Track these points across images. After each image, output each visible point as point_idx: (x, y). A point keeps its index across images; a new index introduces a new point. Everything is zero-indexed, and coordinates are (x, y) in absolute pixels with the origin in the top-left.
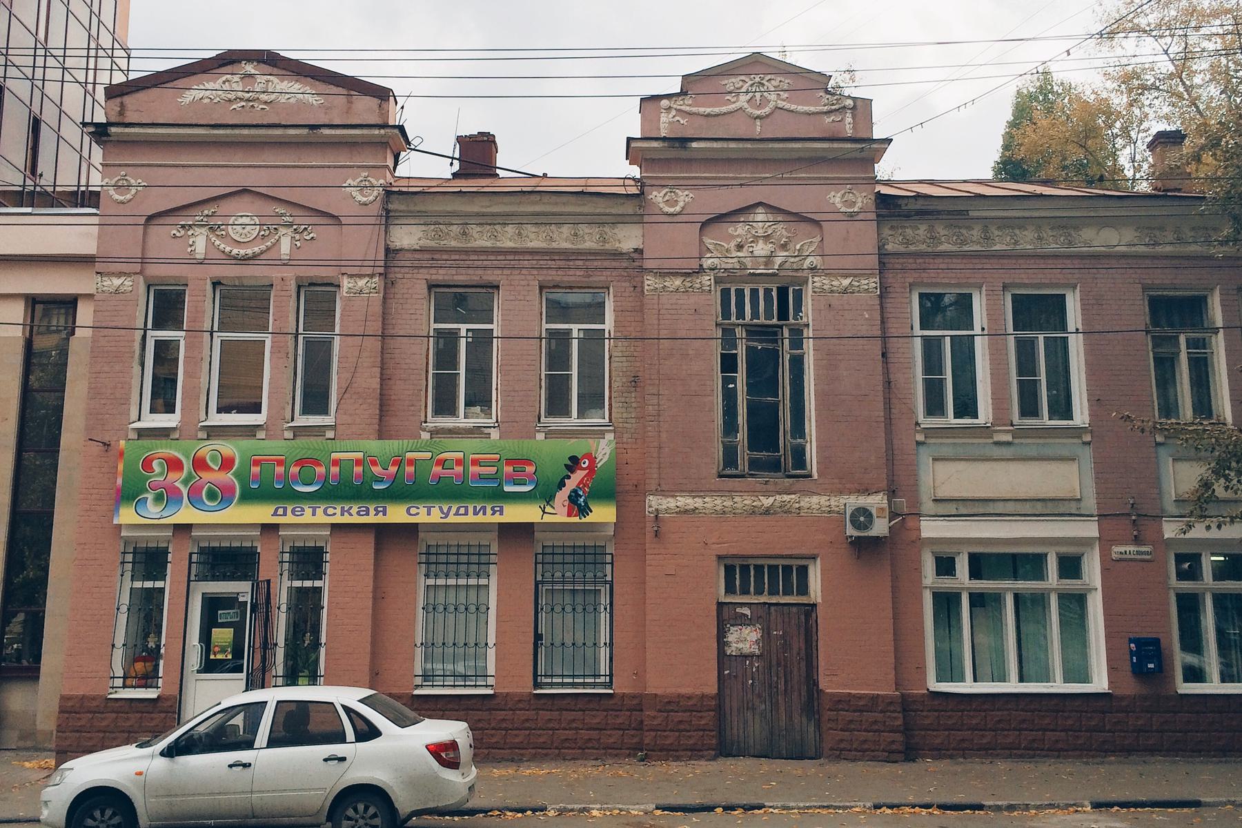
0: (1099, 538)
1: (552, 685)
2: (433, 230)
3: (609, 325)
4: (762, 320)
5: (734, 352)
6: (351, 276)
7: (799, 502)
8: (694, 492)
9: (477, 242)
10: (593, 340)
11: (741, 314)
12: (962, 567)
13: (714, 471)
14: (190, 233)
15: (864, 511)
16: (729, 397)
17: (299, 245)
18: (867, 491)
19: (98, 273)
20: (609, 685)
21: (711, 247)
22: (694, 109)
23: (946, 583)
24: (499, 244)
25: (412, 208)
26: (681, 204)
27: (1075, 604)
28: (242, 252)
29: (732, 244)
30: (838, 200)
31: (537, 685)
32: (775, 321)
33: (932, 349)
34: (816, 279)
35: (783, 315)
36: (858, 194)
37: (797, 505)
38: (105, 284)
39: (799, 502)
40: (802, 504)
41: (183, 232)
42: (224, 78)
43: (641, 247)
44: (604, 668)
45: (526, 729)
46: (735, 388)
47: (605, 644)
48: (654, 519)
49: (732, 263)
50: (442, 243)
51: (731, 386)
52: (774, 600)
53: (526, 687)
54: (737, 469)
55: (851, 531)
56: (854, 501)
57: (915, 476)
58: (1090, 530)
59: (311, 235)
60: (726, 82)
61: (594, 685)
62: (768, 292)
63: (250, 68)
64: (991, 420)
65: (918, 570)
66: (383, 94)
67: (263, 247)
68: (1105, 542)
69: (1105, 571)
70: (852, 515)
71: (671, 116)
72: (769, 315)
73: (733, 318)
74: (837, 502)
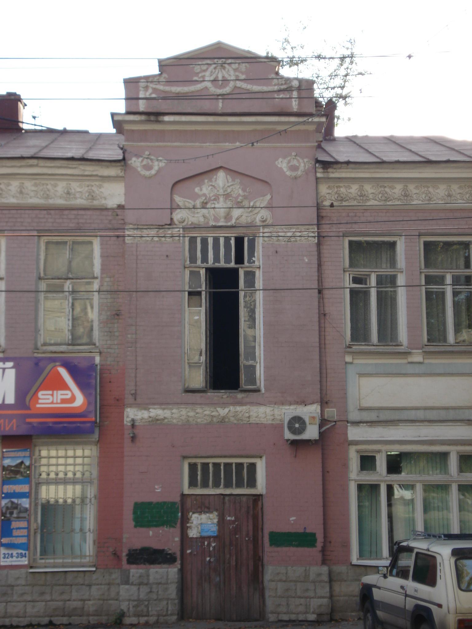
4: (222, 264)
8: (163, 404)
11: (205, 259)
23: (368, 478)
26: (156, 168)
29: (198, 203)
32: (232, 265)
35: (240, 259)
40: (251, 414)
52: (228, 491)
55: (288, 435)
65: (345, 466)
72: (228, 260)
73: (199, 262)
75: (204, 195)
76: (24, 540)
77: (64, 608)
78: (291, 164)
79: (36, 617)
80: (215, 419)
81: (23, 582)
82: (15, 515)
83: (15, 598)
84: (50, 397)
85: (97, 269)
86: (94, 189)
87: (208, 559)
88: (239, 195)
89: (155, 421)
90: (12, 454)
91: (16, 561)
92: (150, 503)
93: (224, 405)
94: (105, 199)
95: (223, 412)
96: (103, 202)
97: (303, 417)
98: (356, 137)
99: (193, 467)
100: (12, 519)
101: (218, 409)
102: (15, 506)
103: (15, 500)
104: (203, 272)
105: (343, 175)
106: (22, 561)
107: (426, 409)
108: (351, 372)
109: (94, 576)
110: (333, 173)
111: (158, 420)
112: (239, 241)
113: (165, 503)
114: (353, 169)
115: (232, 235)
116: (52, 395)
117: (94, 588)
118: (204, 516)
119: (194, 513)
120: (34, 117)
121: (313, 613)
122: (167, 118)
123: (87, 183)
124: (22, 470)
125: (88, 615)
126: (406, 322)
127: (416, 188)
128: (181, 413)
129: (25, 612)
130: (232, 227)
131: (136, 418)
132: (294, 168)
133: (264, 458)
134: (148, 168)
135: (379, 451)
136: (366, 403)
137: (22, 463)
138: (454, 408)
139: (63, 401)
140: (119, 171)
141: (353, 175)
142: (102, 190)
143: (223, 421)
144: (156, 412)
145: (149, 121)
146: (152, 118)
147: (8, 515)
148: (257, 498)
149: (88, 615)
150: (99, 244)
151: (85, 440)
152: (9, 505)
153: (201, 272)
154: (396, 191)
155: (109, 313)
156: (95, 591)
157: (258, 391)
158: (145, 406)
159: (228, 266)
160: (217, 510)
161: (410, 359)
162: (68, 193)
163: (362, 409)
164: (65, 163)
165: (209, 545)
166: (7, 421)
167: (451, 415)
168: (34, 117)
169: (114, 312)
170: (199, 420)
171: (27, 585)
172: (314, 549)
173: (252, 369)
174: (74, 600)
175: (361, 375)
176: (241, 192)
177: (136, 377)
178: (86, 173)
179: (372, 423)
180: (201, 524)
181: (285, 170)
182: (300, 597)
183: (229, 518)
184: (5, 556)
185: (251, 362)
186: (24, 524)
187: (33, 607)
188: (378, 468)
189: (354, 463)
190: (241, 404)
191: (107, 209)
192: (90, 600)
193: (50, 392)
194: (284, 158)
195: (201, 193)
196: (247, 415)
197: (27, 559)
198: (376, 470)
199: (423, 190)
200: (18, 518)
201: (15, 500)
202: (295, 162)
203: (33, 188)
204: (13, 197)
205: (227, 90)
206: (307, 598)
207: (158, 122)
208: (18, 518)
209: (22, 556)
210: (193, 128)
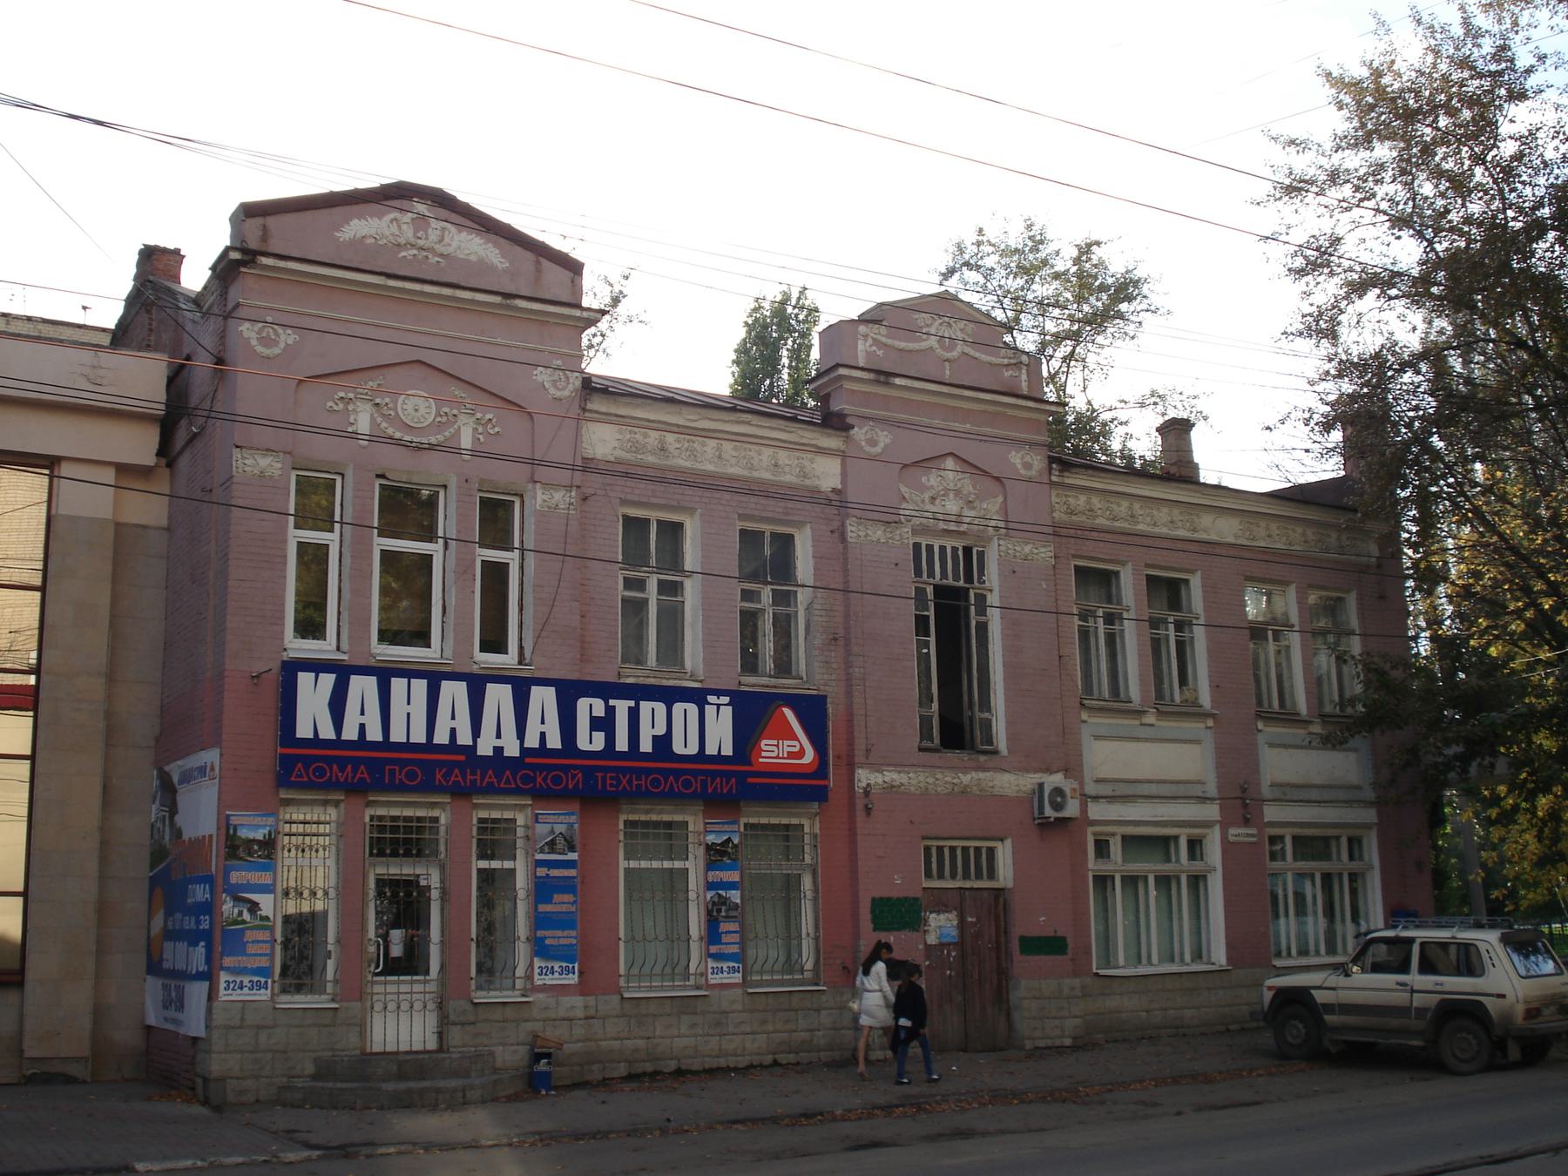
0: (168, 529)
2: (629, 441)
4: (950, 581)
5: (926, 613)
6: (545, 485)
7: (992, 781)
8: (899, 766)
9: (675, 461)
11: (931, 574)
12: (1116, 848)
14: (351, 407)
16: (924, 660)
17: (482, 440)
19: (237, 447)
22: (890, 342)
23: (1104, 867)
24: (698, 466)
26: (882, 445)
27: (1197, 881)
29: (927, 496)
32: (961, 583)
34: (1001, 542)
35: (969, 579)
37: (991, 784)
38: (247, 462)
39: (992, 781)
40: (995, 782)
41: (341, 406)
42: (392, 216)
43: (839, 487)
47: (808, 935)
48: (863, 795)
50: (639, 457)
52: (968, 884)
54: (933, 742)
58: (1212, 812)
60: (917, 316)
62: (955, 550)
63: (421, 208)
68: (1225, 825)
69: (1224, 852)
72: (957, 578)
74: (1028, 781)
75: (932, 487)
76: (735, 949)
77: (671, 1048)
79: (758, 1054)
80: (956, 789)
81: (740, 1007)
82: (723, 914)
83: (731, 1029)
84: (775, 748)
86: (806, 463)
87: (948, 972)
88: (970, 493)
89: (890, 788)
90: (717, 828)
91: (249, 994)
92: (889, 899)
93: (965, 770)
94: (819, 479)
95: (966, 779)
96: (817, 482)
97: (1064, 788)
98: (168, 377)
100: (721, 919)
101: (960, 775)
102: (723, 901)
103: (722, 893)
104: (930, 590)
105: (1078, 482)
106: (260, 995)
107: (1159, 782)
108: (1086, 732)
109: (824, 998)
110: (1068, 477)
111: (893, 786)
112: (968, 551)
113: (906, 898)
114: (1088, 476)
115: (959, 544)
116: (777, 746)
117: (824, 1013)
118: (942, 917)
119: (931, 913)
121: (1069, 1037)
122: (898, 381)
123: (797, 454)
124: (730, 850)
125: (819, 1050)
126: (1137, 673)
127: (1141, 508)
128: (920, 778)
129: (744, 1048)
131: (872, 782)
132: (1028, 466)
135: (1113, 835)
137: (729, 840)
139: (791, 755)
140: (841, 444)
141: (1088, 484)
142: (814, 465)
143: (965, 791)
144: (891, 776)
145: (878, 382)
146: (882, 378)
147: (715, 914)
148: (999, 892)
149: (819, 1050)
150: (809, 544)
151: (803, 811)
152: (716, 899)
153: (928, 590)
154: (1122, 509)
155: (824, 637)
156: (825, 1018)
157: (995, 752)
158: (877, 767)
159: (956, 584)
160: (955, 909)
162: (776, 465)
163: (1098, 781)
164: (782, 423)
165: (949, 953)
166: (479, 784)
167: (1181, 790)
169: (831, 637)
170: (939, 789)
171: (744, 1011)
172: (1065, 957)
173: (987, 725)
174: (801, 1031)
175: (1097, 738)
176: (971, 489)
177: (866, 727)
179: (1111, 799)
180: (940, 927)
182: (1055, 1018)
183: (970, 919)
184: (228, 985)
185: (986, 715)
186: (734, 926)
187: (754, 1040)
188: (1112, 856)
190: (985, 769)
192: (629, 1039)
193: (775, 742)
195: (928, 484)
197: (740, 975)
198: (1109, 857)
199: (1147, 511)
200: (726, 917)
201: (722, 893)
202: (1028, 459)
205: (954, 354)
206: (1061, 1018)
207: (887, 384)
208: (726, 917)
209: (734, 970)
210: (927, 398)
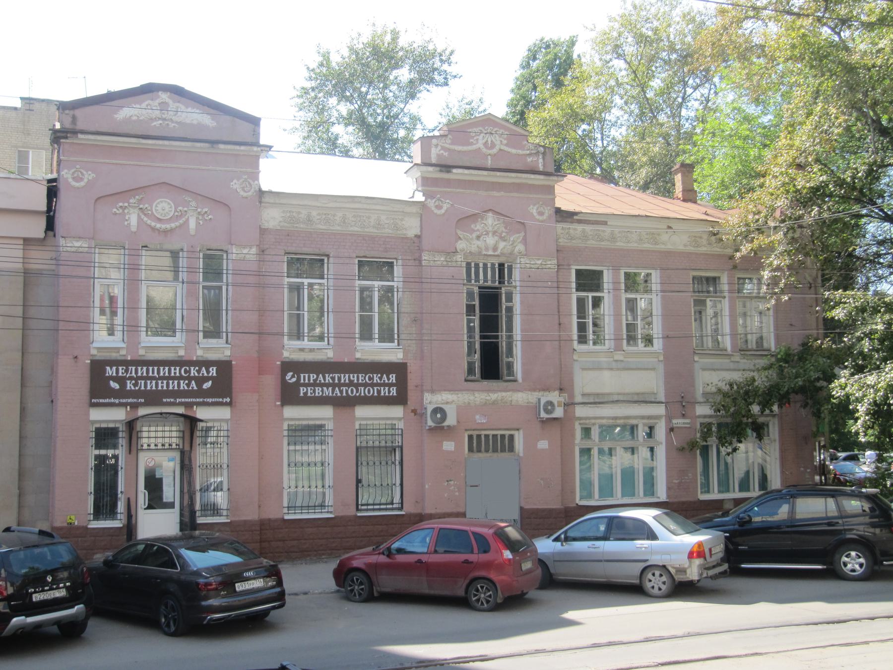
1: (367, 510)
3: (397, 282)
4: (489, 283)
10: (387, 295)
13: (463, 379)
15: (551, 403)
18: (546, 389)
20: (401, 509)
21: (461, 236)
23: (587, 444)
25: (277, 201)
28: (163, 226)
29: (474, 235)
30: (535, 211)
31: (358, 509)
33: (581, 303)
36: (85, 173)
41: (121, 211)
44: (397, 499)
45: (353, 537)
46: (474, 326)
49: (474, 249)
51: (472, 324)
53: (351, 511)
55: (543, 415)
56: (545, 397)
57: (572, 381)
58: (661, 410)
59: (210, 217)
61: (392, 509)
64: (613, 347)
65: (573, 436)
66: (254, 122)
67: (177, 224)
68: (669, 418)
70: (544, 405)
71: (438, 150)
72: (493, 281)
73: (473, 282)
78: (539, 210)
85: (201, 266)
88: (502, 232)
93: (494, 391)
95: (494, 396)
99: (470, 437)
112: (501, 265)
115: (496, 262)
120: (669, 227)
122: (455, 171)
130: (498, 256)
132: (541, 214)
133: (521, 432)
134: (439, 207)
135: (594, 424)
136: (587, 390)
138: (643, 394)
143: (494, 403)
157: (515, 381)
161: (732, 359)
163: (583, 395)
168: (669, 227)
173: (510, 366)
176: (504, 230)
178: (395, 210)
181: (535, 214)
185: (510, 359)
189: (578, 434)
191: (407, 238)
194: (534, 205)
196: (510, 399)
202: (541, 209)
203: (353, 219)
204: (339, 225)
